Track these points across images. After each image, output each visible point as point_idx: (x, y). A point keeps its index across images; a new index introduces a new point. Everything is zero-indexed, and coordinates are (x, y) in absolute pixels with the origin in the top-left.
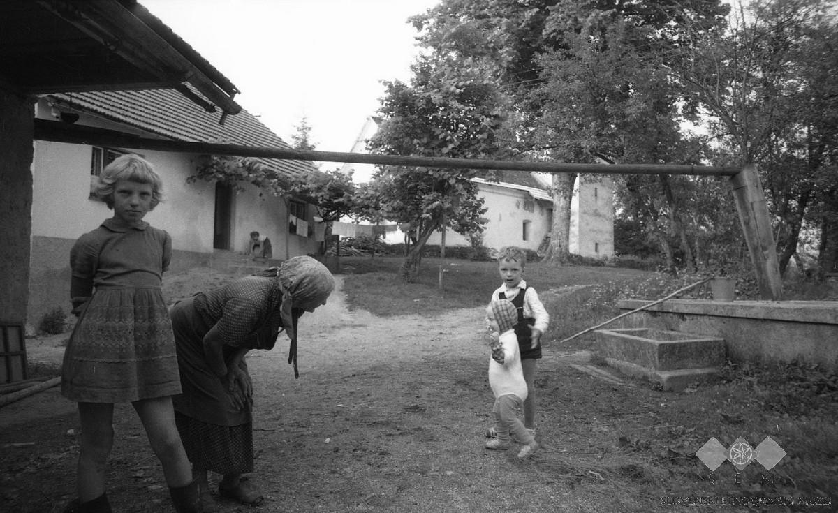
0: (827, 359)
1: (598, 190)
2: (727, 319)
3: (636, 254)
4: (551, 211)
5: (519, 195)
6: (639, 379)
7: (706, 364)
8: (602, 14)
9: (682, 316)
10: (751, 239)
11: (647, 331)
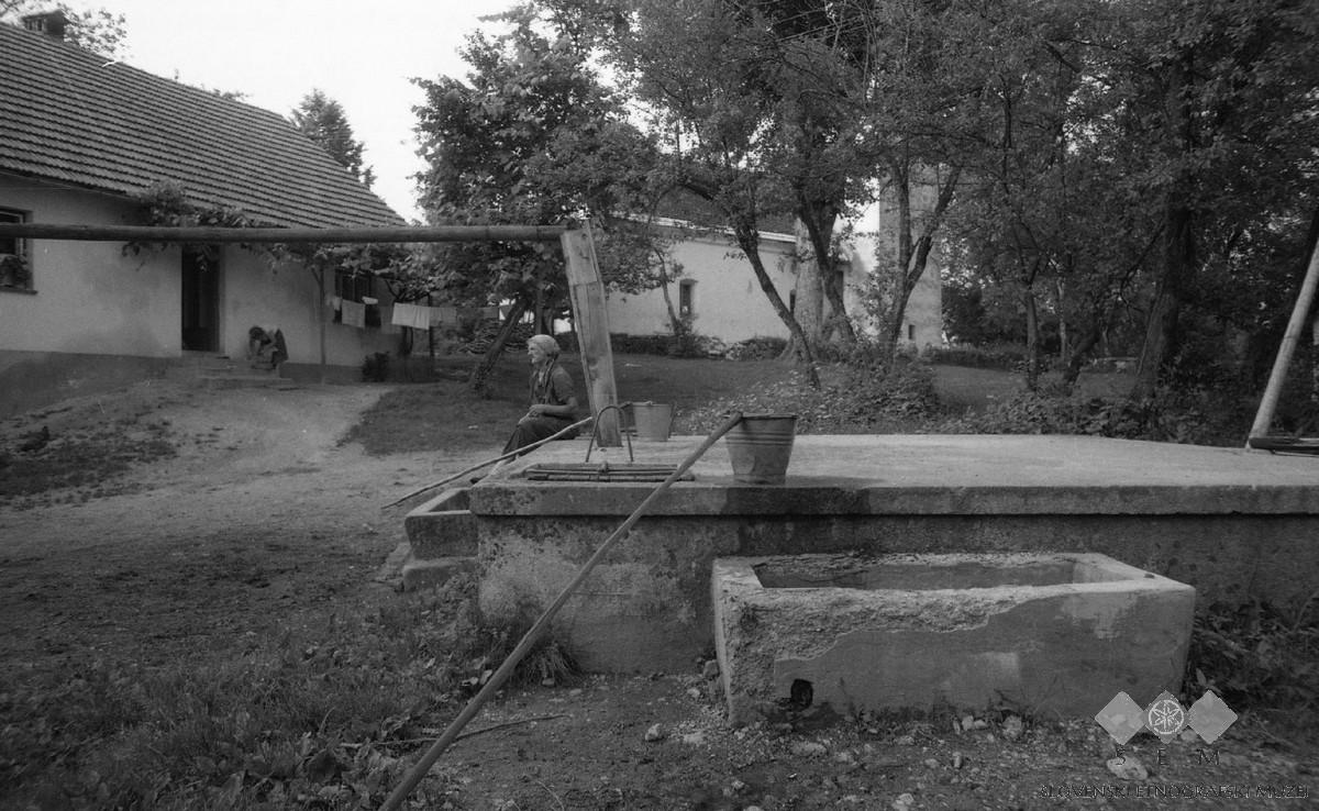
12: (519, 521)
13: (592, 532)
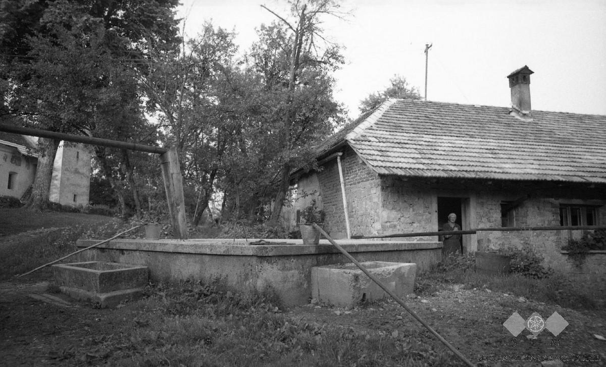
0: (205, 277)
1: (79, 154)
2: (151, 253)
3: (106, 204)
4: (35, 166)
5: (8, 150)
6: (84, 301)
7: (135, 285)
8: (92, 19)
9: (122, 251)
10: (170, 197)
11: (96, 263)
12: (267, 258)
13: (284, 260)
